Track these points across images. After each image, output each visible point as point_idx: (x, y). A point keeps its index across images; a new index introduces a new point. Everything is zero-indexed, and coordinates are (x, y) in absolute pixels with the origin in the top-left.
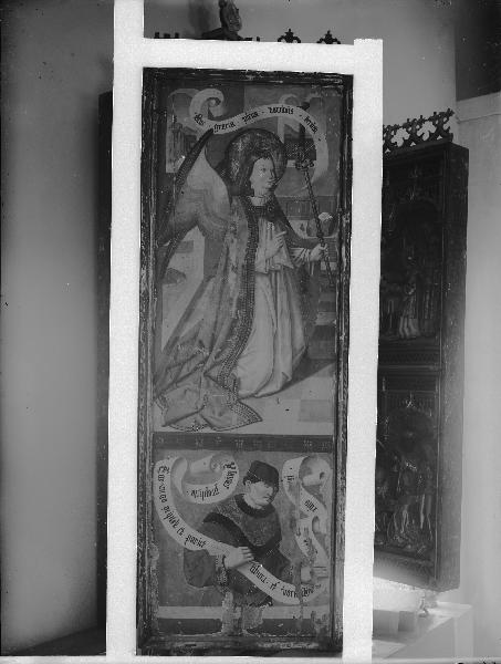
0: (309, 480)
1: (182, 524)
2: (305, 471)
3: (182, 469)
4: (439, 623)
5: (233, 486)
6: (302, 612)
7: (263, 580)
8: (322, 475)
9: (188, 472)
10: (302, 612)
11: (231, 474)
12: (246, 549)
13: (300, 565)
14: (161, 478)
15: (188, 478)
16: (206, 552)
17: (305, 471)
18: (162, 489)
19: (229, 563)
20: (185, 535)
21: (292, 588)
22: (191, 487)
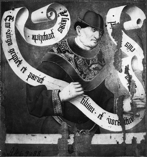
0: (128, 25)
1: (25, 64)
2: (125, 17)
3: (25, 16)
4: (123, 116)
5: (65, 32)
6: (124, 138)
7: (95, 113)
8: (138, 21)
9: (29, 19)
10: (124, 138)
11: (64, 20)
12: (77, 85)
13: (123, 98)
14: (8, 26)
15: (30, 25)
16: (44, 87)
17: (125, 17)
18: (8, 34)
19: (64, 96)
20: (27, 73)
21: (115, 117)
22: (32, 32)
